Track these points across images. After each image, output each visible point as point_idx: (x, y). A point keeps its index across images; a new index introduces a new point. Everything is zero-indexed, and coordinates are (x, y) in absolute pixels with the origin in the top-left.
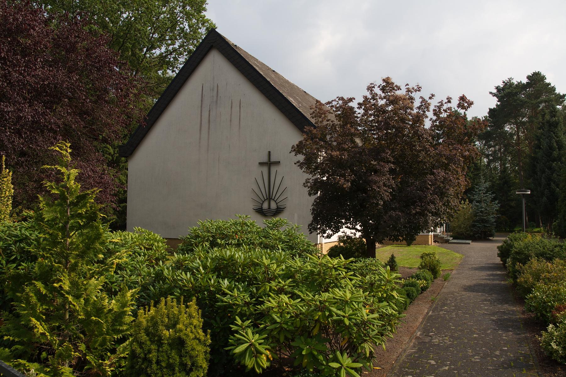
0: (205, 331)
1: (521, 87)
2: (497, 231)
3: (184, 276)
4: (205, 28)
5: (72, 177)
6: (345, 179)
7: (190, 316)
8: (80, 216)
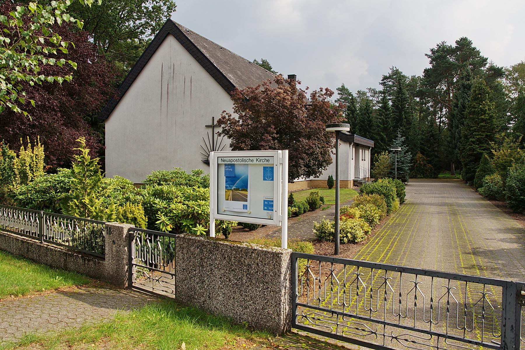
0: (145, 216)
1: (451, 51)
2: (411, 178)
3: (139, 198)
4: (166, 7)
5: (87, 153)
6: (245, 145)
7: (139, 209)
8: (91, 171)
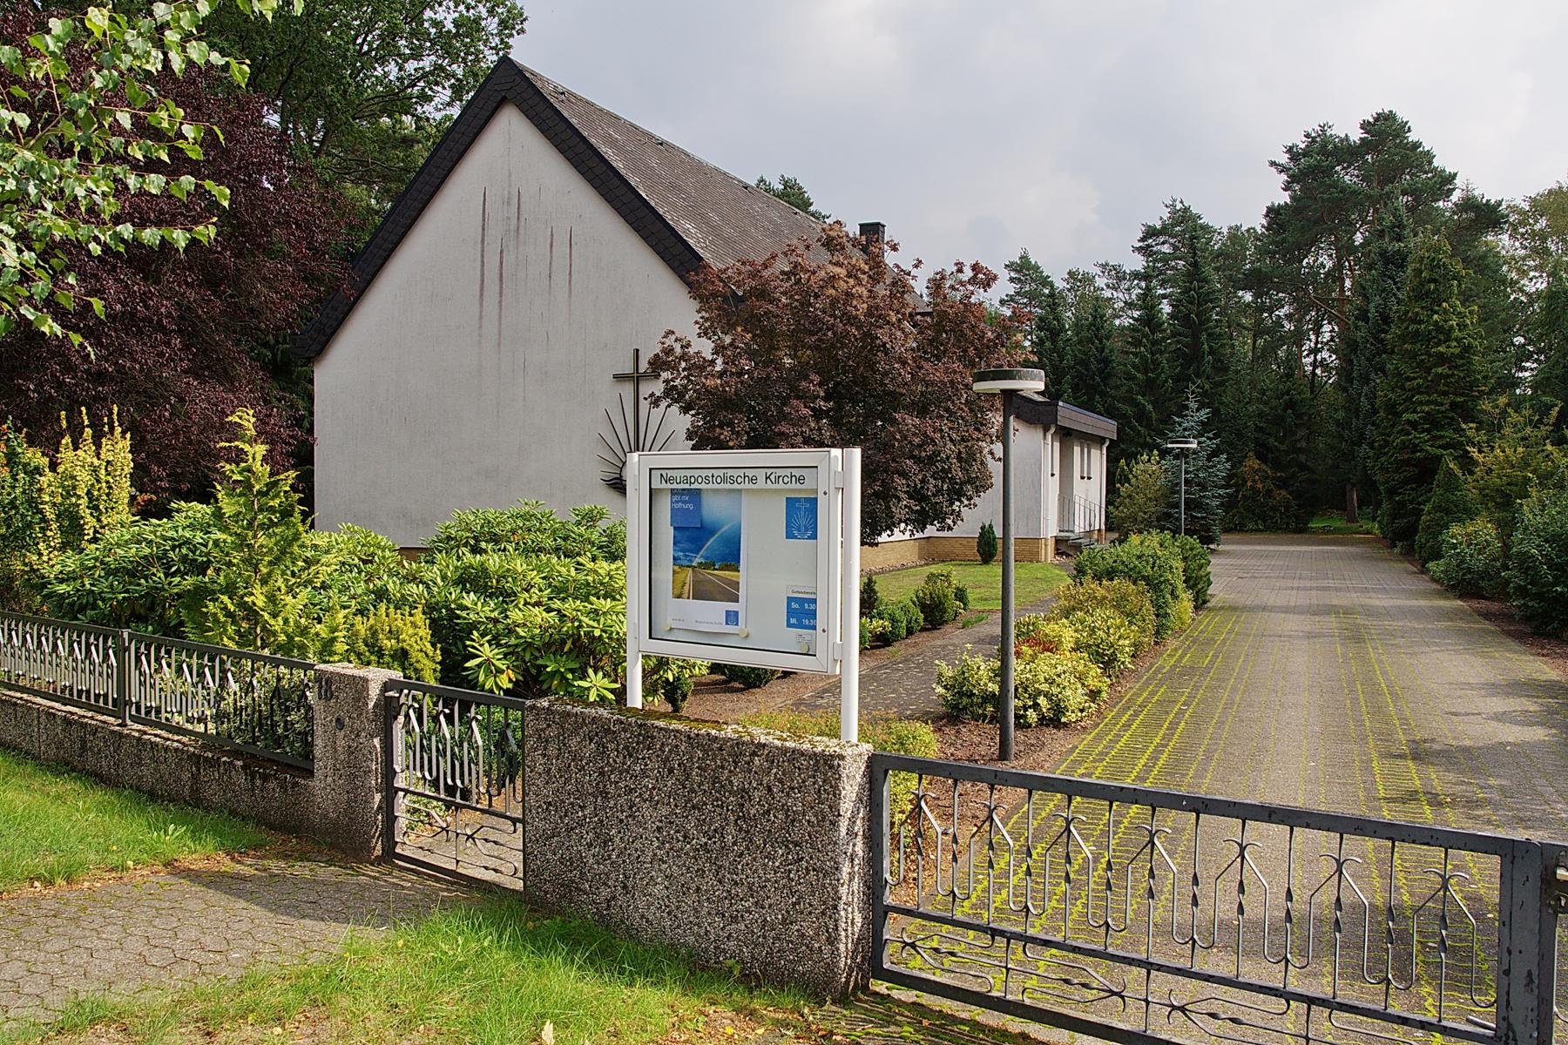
0: (434, 645)
1: (1346, 152)
2: (1226, 531)
3: (415, 590)
5: (259, 458)
8: (272, 510)
